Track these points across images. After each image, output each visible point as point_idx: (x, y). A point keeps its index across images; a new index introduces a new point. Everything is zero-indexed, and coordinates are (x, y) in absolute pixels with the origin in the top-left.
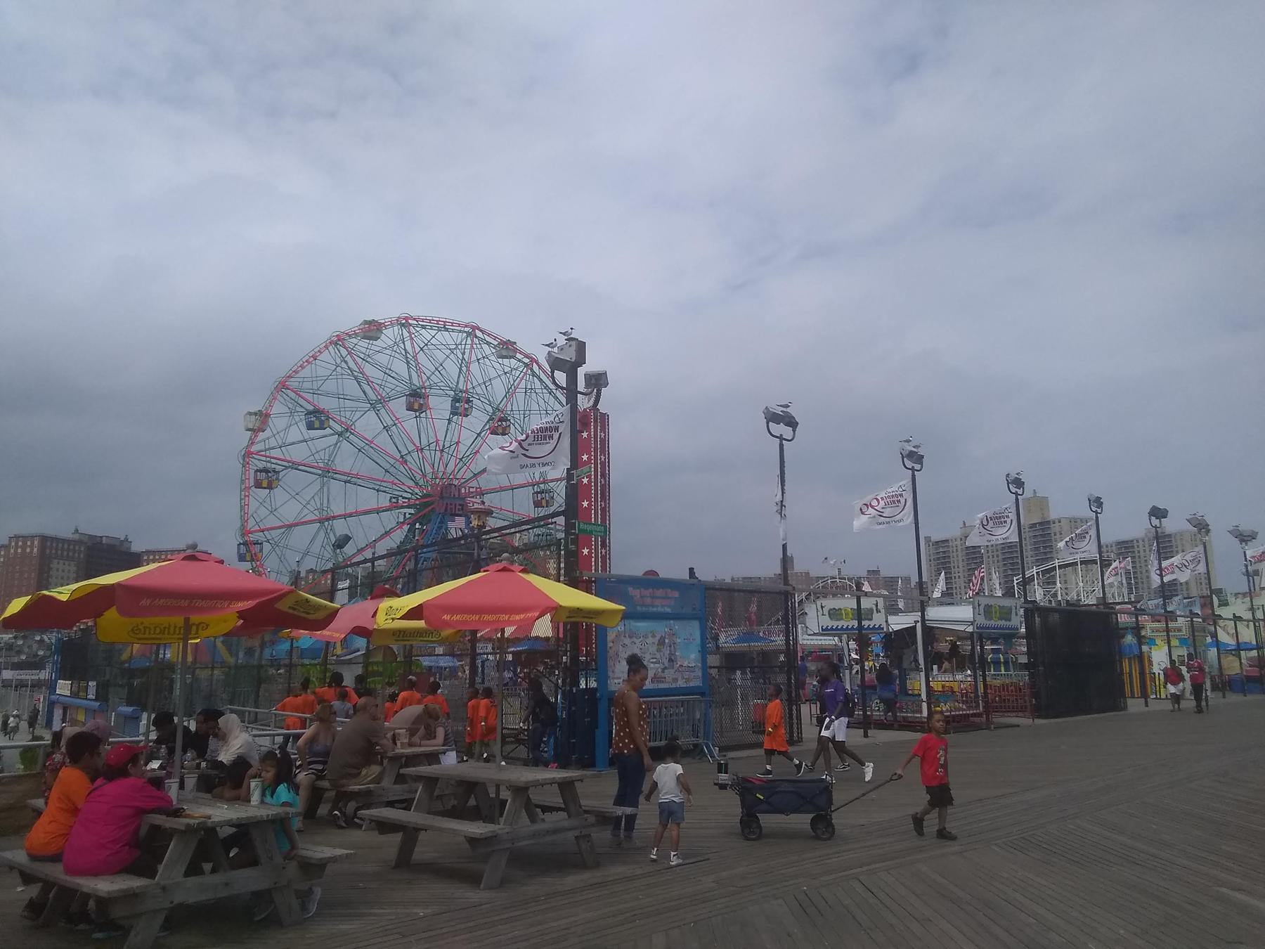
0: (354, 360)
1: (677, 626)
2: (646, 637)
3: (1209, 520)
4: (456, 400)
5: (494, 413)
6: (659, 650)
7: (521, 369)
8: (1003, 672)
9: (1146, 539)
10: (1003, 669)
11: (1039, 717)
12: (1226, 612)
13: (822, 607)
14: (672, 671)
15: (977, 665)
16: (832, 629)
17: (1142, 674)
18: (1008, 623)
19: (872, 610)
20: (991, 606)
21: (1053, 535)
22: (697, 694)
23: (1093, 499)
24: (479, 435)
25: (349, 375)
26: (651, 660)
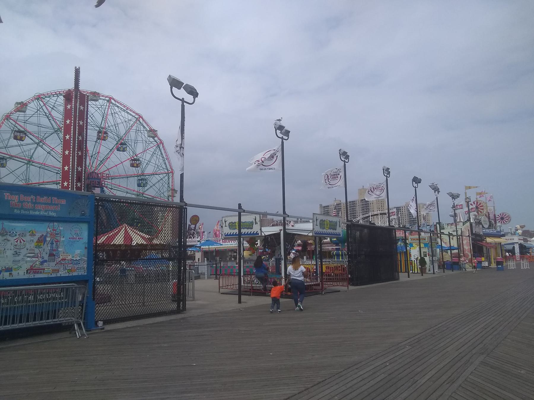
0: (47, 108)
1: (61, 227)
2: (23, 235)
3: (439, 186)
4: (99, 132)
5: (119, 141)
6: (38, 247)
7: (105, 105)
8: (341, 260)
9: (406, 207)
10: (341, 258)
11: (353, 285)
12: (446, 231)
13: (225, 222)
14: (53, 264)
15: (318, 256)
16: (230, 235)
17: (406, 261)
18: (334, 231)
19: (252, 222)
20: (324, 220)
21: (370, 204)
22: (74, 282)
23: (386, 169)
24: (111, 150)
25: (43, 115)
26: (28, 255)
